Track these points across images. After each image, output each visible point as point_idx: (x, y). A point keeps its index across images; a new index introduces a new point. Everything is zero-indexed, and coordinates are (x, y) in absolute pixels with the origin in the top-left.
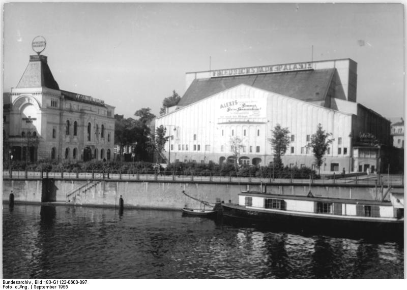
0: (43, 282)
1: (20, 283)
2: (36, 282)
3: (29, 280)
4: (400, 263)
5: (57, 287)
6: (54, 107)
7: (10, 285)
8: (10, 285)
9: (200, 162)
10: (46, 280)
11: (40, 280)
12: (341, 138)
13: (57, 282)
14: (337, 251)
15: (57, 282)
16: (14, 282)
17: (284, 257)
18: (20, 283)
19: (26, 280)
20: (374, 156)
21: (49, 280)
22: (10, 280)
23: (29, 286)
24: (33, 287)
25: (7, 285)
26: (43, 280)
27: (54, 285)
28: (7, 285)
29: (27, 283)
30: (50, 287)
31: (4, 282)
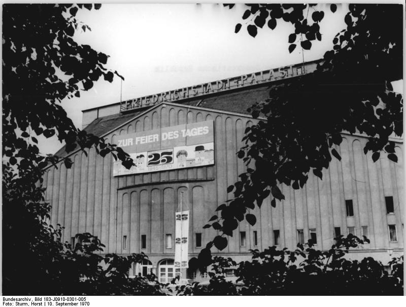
0: (43, 299)
1: (20, 300)
2: (36, 299)
3: (29, 297)
4: (287, 18)
5: (79, 304)
6: (395, 241)
7: (10, 302)
8: (10, 302)
9: (335, 241)
10: (46, 297)
11: (40, 297)
12: (200, 234)
13: (61, 299)
14: (297, 252)
15: (61, 299)
16: (14, 299)
17: (342, 238)
18: (20, 300)
19: (26, 297)
20: (310, 238)
21: (49, 297)
22: (10, 297)
23: (29, 303)
24: (47, 304)
25: (7, 302)
26: (43, 297)
27: (76, 302)
28: (7, 302)
29: (27, 300)
30: (72, 304)
31: (4, 299)
